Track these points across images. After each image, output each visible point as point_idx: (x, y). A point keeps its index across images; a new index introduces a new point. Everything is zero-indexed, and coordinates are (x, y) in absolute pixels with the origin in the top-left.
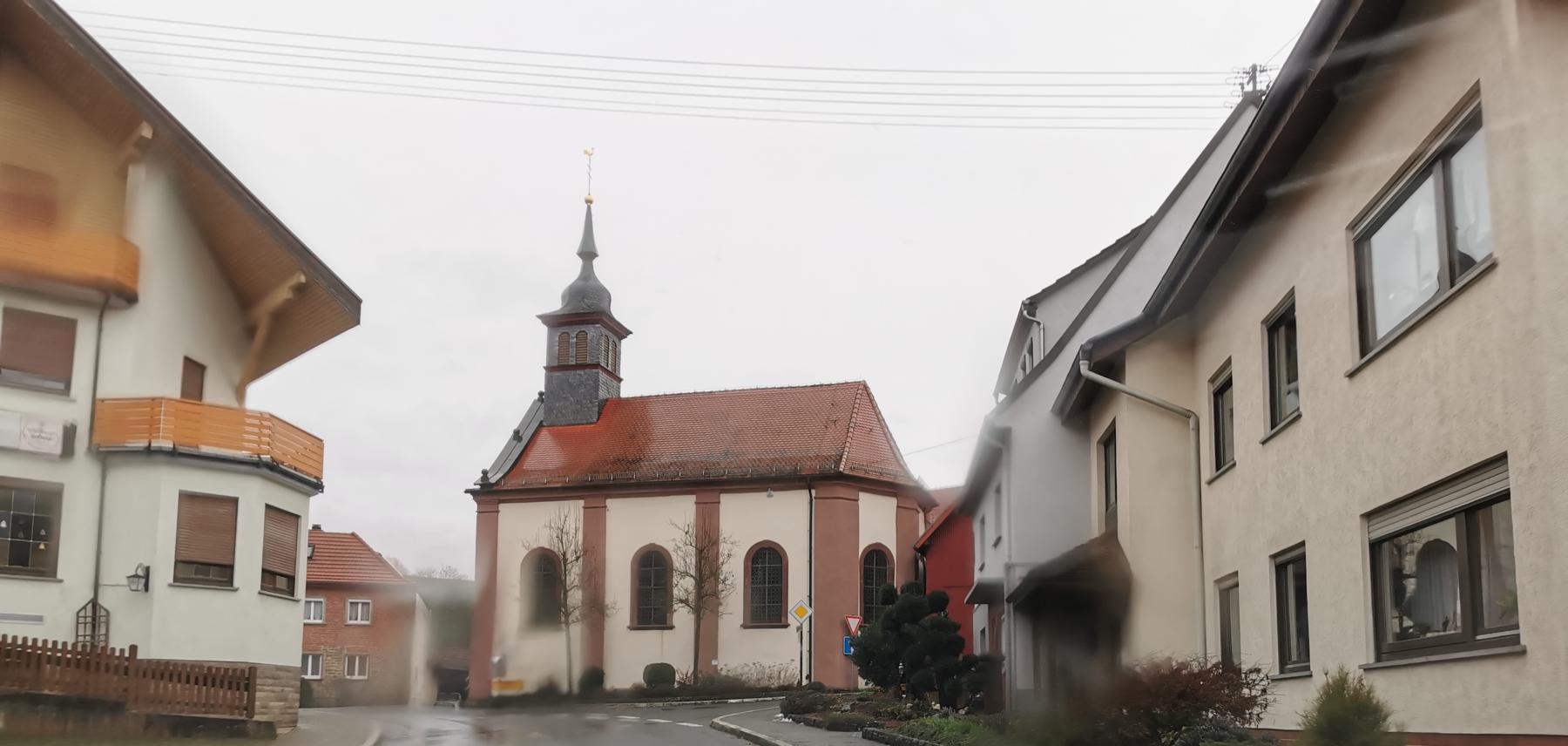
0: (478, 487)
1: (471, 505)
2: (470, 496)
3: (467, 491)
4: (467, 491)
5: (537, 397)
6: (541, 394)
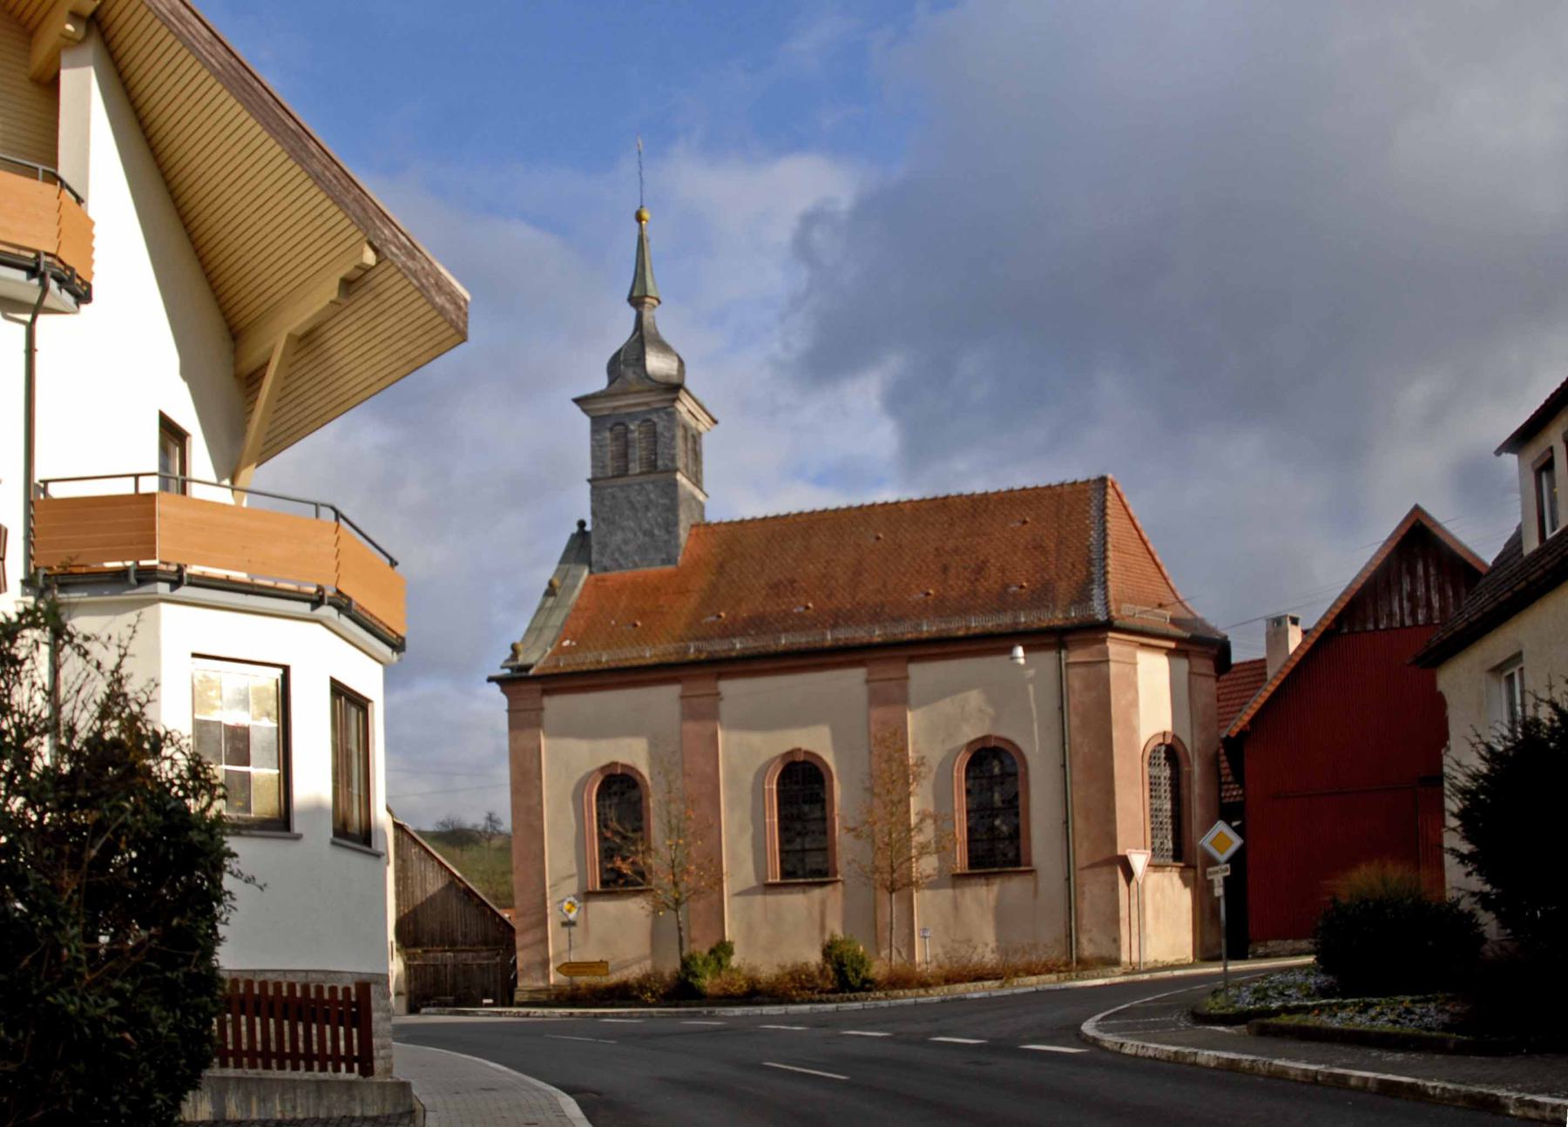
0: (507, 671)
1: (496, 702)
2: (495, 687)
3: (490, 680)
4: (490, 680)
5: (575, 529)
6: (582, 524)
